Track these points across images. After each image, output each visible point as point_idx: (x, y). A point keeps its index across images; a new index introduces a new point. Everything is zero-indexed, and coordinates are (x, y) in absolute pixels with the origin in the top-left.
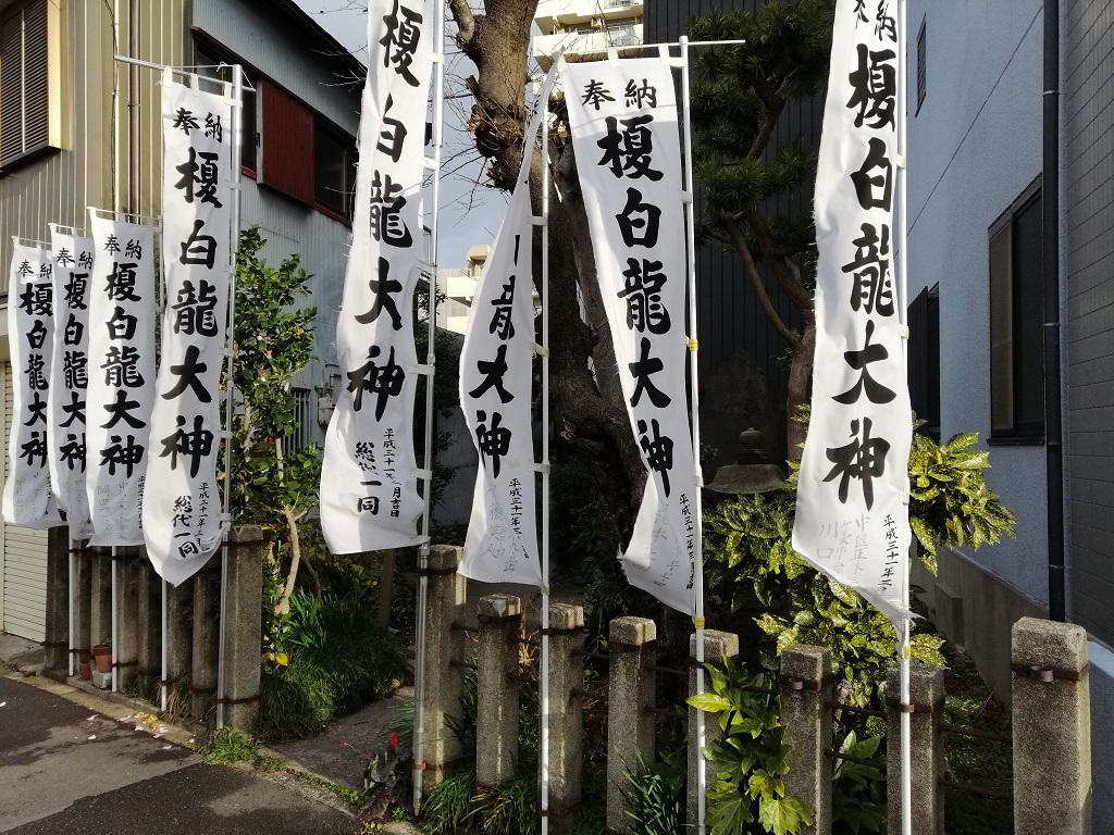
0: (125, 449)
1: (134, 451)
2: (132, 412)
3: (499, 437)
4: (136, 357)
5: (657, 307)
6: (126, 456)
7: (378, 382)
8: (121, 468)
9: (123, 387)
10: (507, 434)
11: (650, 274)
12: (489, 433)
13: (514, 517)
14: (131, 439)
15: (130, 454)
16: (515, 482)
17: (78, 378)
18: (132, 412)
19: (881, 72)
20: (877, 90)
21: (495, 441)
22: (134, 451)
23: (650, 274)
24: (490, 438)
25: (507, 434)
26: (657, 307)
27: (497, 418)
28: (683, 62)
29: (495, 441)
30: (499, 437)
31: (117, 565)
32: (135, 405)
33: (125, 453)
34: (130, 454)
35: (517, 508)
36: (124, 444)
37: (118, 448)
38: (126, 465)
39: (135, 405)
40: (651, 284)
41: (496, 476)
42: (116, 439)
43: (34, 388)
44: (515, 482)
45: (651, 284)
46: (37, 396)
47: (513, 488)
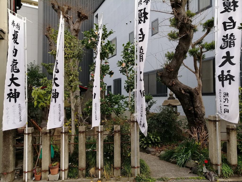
0: (14, 93)
1: (17, 94)
2: (15, 81)
3: (56, 94)
4: (17, 63)
5: (57, 68)
6: (14, 96)
7: (225, 77)
8: (13, 100)
9: (13, 73)
10: (58, 93)
11: (15, 62)
12: (54, 94)
13: (20, 112)
14: (15, 90)
15: (15, 95)
16: (60, 105)
17: (14, 69)
18: (15, 81)
19: (16, 34)
20: (15, 37)
21: (55, 95)
22: (17, 94)
23: (15, 62)
24: (54, 95)
25: (58, 93)
26: (57, 68)
27: (15, 90)
28: (25, 22)
29: (55, 95)
30: (56, 94)
31: (65, 136)
32: (17, 79)
33: (14, 94)
34: (15, 95)
35: (60, 110)
36: (13, 92)
37: (11, 93)
38: (14, 99)
39: (17, 79)
40: (15, 64)
41: (55, 103)
42: (11, 90)
43: (12, 72)
44: (60, 105)
45: (15, 64)
46: (13, 75)
47: (59, 106)
